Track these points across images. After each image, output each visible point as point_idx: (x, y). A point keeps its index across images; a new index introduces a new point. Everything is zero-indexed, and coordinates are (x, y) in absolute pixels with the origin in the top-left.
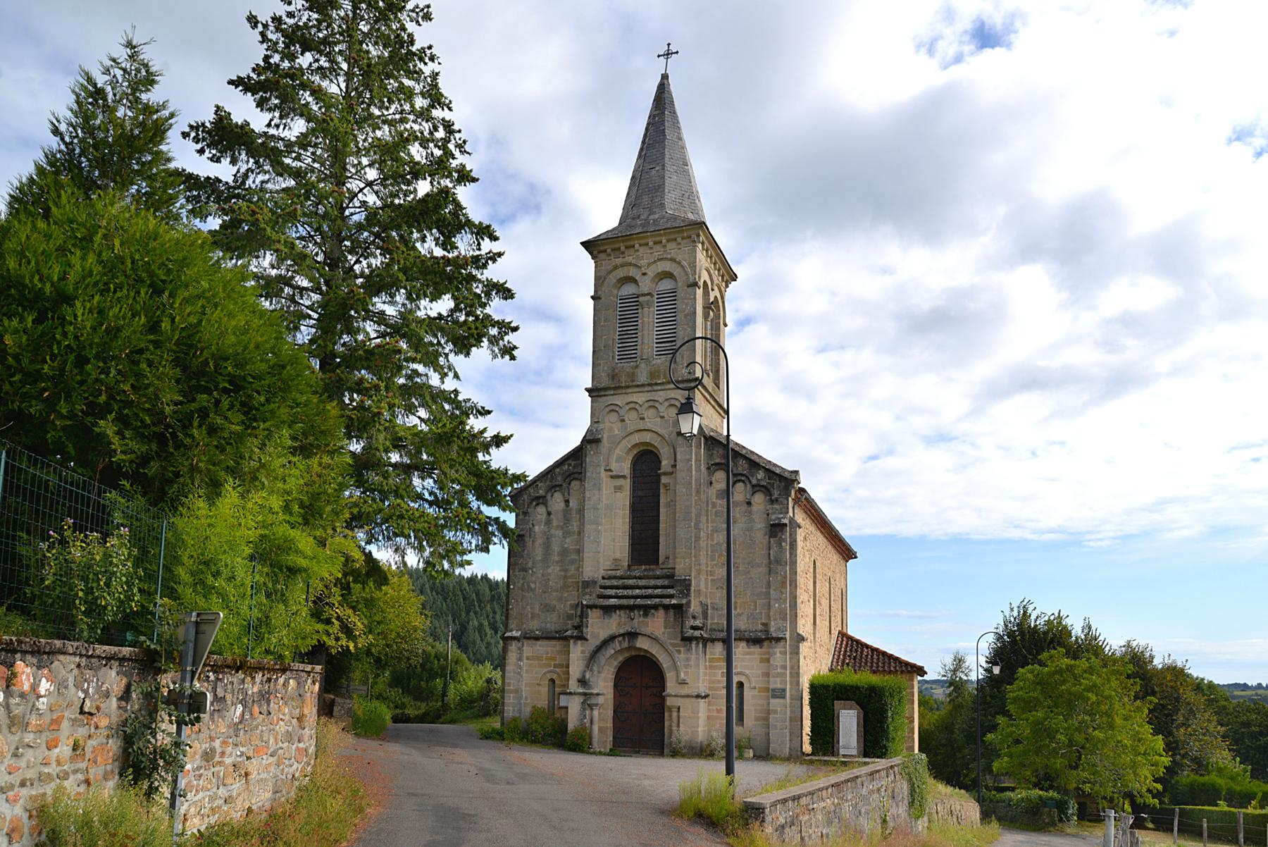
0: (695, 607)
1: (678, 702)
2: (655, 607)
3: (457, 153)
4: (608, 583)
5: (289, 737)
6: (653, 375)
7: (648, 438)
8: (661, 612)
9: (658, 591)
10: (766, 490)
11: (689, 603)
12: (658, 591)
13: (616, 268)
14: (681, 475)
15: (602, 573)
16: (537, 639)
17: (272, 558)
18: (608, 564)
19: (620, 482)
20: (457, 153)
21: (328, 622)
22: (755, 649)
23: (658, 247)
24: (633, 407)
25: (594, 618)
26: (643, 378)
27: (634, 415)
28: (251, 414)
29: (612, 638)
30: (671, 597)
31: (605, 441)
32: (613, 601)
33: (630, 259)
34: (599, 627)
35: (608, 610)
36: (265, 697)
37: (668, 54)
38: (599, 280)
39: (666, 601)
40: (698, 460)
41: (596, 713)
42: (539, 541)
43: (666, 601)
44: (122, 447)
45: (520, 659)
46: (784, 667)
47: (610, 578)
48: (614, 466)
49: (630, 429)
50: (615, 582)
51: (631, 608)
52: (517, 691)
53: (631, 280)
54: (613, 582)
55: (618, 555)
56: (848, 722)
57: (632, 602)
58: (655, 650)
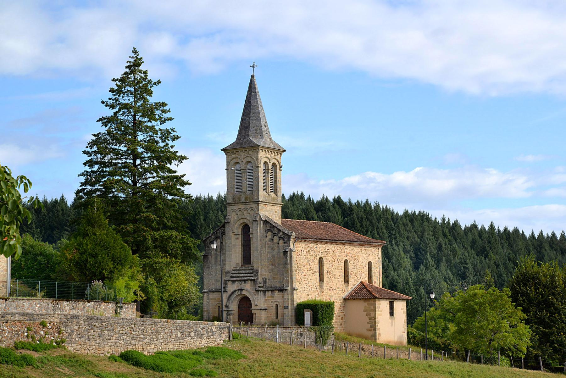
0: (260, 279)
1: (255, 312)
2: (247, 280)
3: (172, 132)
4: (234, 272)
5: (131, 315)
6: (246, 199)
7: (245, 221)
8: (250, 282)
9: (249, 275)
10: (283, 239)
11: (258, 279)
12: (249, 275)
13: (233, 159)
14: (254, 235)
15: (233, 268)
16: (213, 292)
17: (127, 287)
18: (234, 265)
19: (237, 236)
20: (172, 132)
21: (137, 295)
22: (281, 293)
23: (246, 152)
24: (240, 210)
25: (229, 283)
26: (243, 200)
27: (240, 213)
28: (122, 265)
29: (235, 291)
30: (252, 276)
31: (232, 222)
32: (235, 279)
33: (237, 156)
34: (231, 287)
35: (234, 281)
36: (128, 308)
37: (254, 66)
38: (228, 163)
39: (251, 278)
40: (260, 230)
41: (231, 317)
42: (213, 257)
43: (251, 278)
44: (106, 274)
45: (208, 299)
46: (288, 299)
47: (235, 270)
48: (235, 231)
49: (240, 218)
50: (236, 272)
51: (240, 281)
52: (207, 311)
53: (237, 163)
54: (236, 272)
55: (238, 262)
56: (308, 316)
57: (240, 279)
58: (248, 295)
